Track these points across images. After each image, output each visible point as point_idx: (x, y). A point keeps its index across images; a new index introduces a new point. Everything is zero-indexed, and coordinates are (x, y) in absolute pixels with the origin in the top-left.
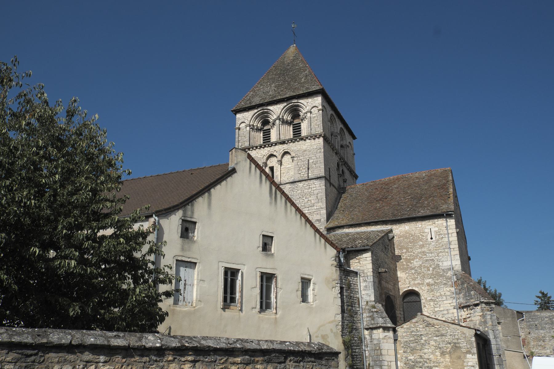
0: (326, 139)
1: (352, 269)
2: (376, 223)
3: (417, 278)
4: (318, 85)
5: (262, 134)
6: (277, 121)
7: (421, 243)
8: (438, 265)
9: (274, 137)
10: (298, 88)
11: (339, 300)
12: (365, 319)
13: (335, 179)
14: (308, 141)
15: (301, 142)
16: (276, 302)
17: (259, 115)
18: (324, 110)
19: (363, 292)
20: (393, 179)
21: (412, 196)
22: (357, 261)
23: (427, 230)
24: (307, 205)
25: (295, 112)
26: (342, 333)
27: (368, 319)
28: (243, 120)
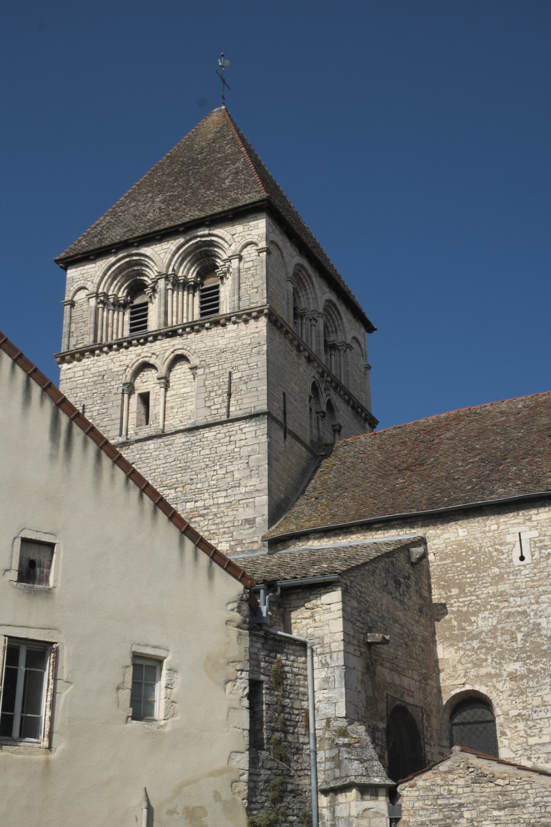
0: (274, 322)
1: (295, 635)
2: (387, 524)
3: (486, 660)
4: (259, 192)
5: (127, 317)
6: (162, 283)
7: (496, 570)
8: (537, 627)
9: (153, 322)
10: (213, 201)
11: (246, 715)
12: (320, 764)
13: (301, 420)
14: (231, 327)
15: (217, 331)
16: (52, 719)
17: (120, 270)
18: (275, 252)
19: (319, 695)
20: (446, 419)
21: (484, 455)
22: (308, 614)
23: (512, 538)
24: (222, 485)
25: (205, 260)
26: (250, 802)
27: (329, 765)
28: (81, 283)
